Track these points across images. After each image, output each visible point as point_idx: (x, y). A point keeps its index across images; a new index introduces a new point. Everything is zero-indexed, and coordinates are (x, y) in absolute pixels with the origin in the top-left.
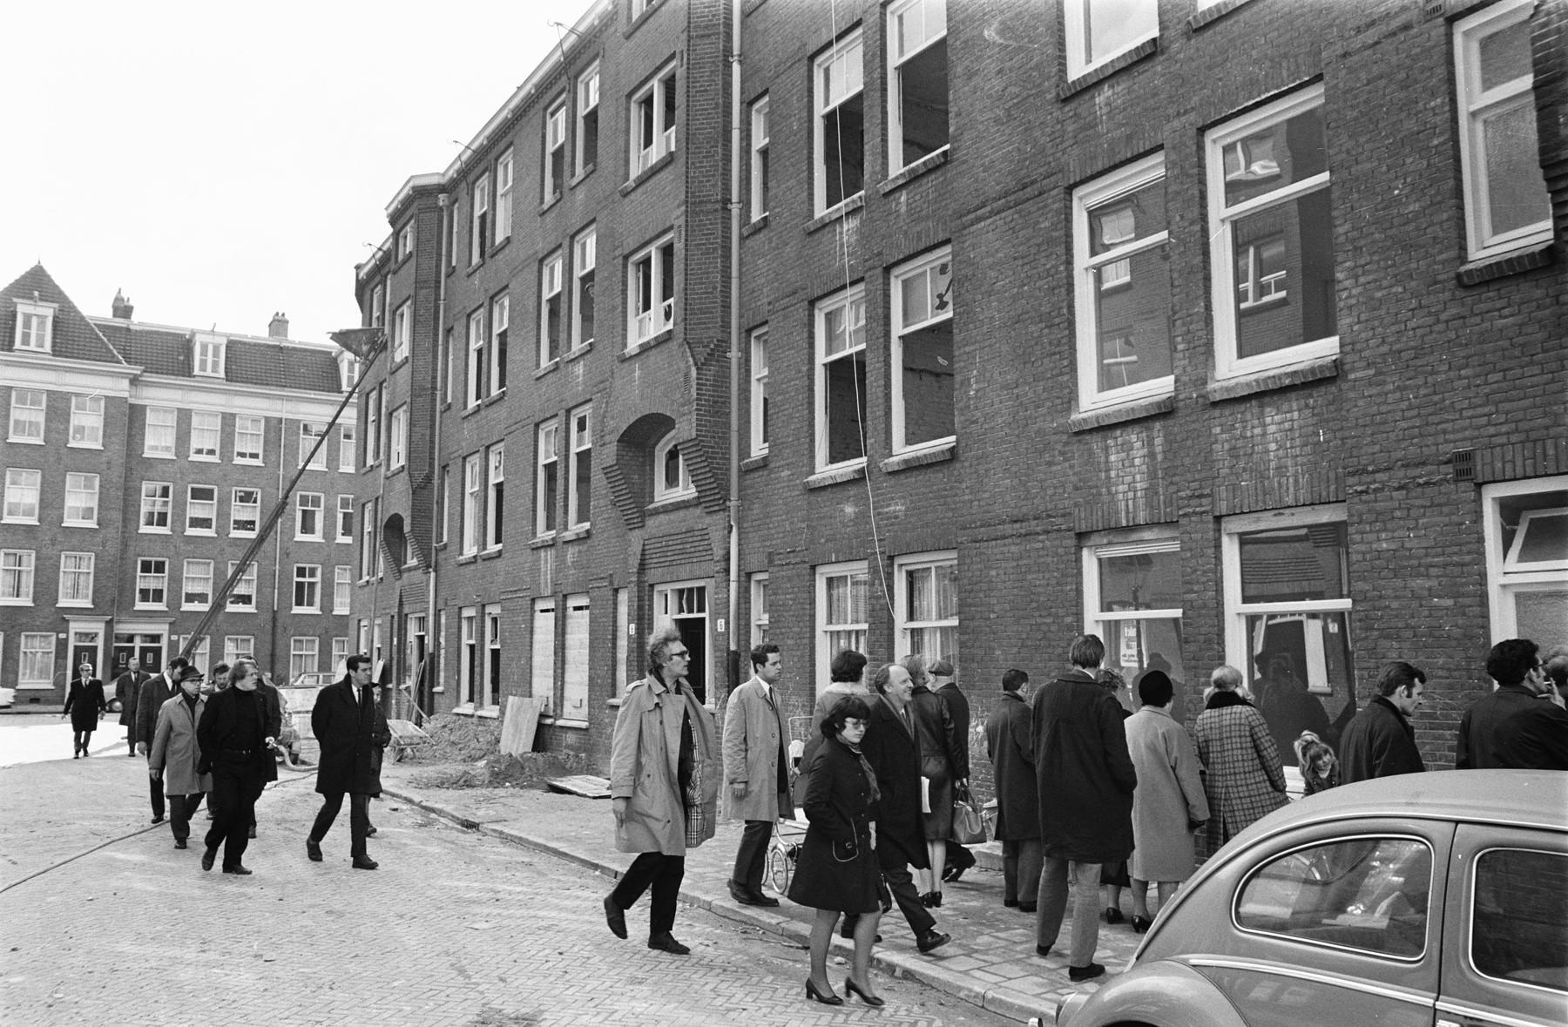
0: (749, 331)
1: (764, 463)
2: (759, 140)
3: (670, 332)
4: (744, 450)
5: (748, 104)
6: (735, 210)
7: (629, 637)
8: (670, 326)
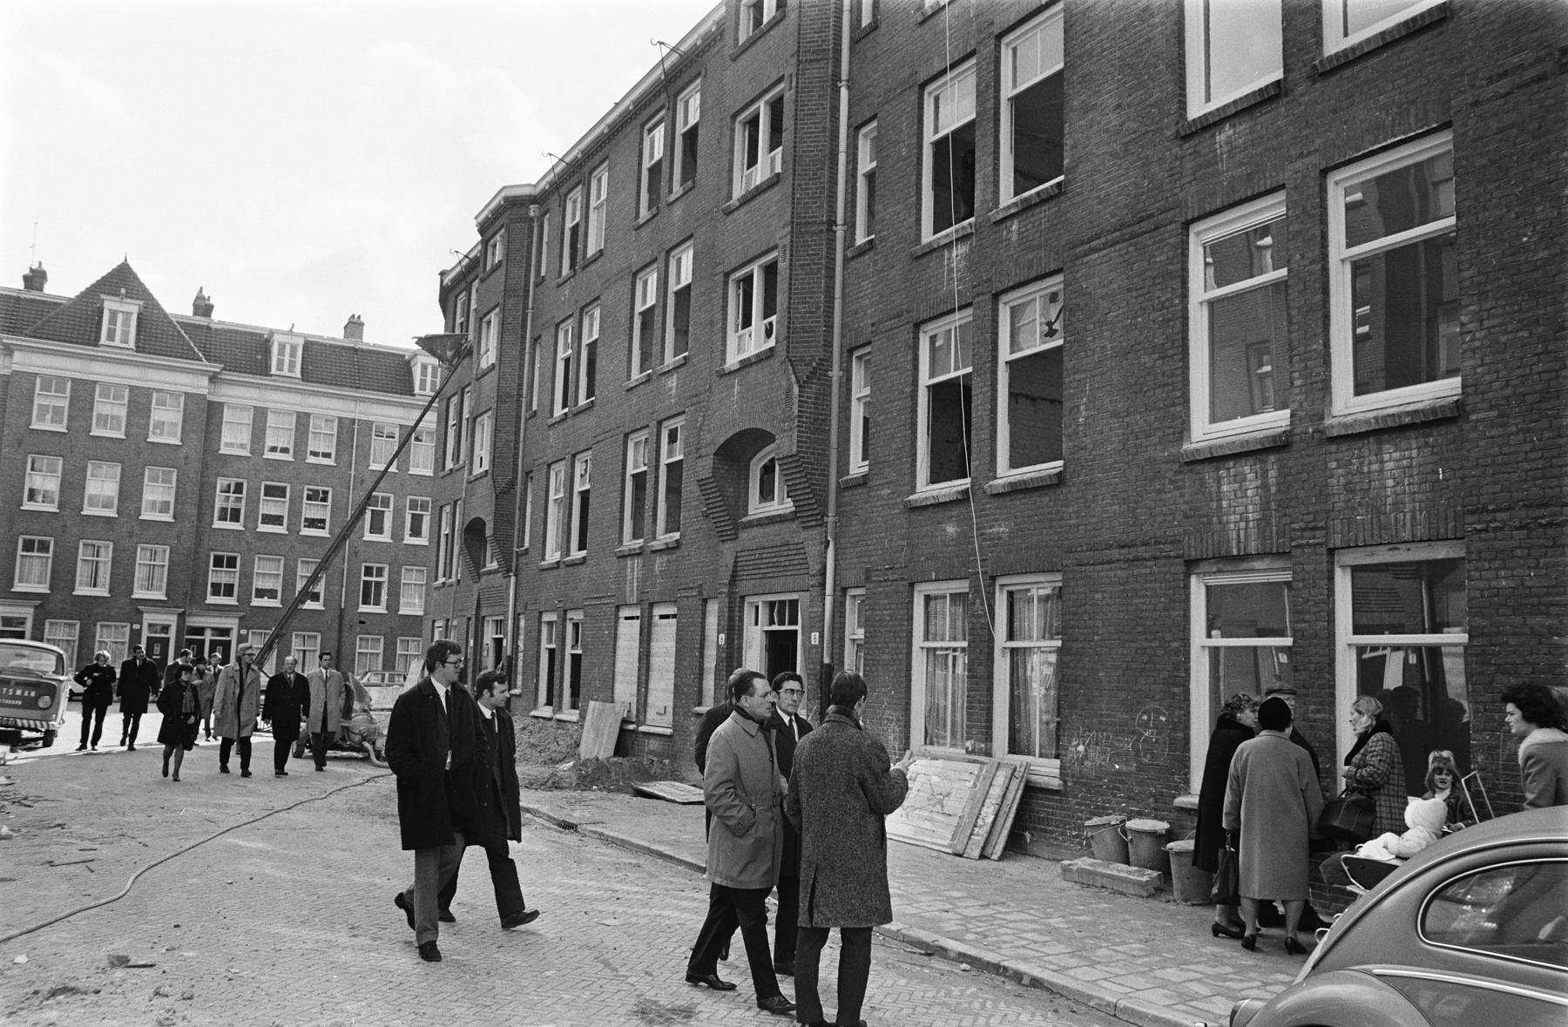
0: (851, 351)
1: (863, 481)
2: (865, 165)
4: (843, 467)
5: (855, 129)
6: (840, 232)
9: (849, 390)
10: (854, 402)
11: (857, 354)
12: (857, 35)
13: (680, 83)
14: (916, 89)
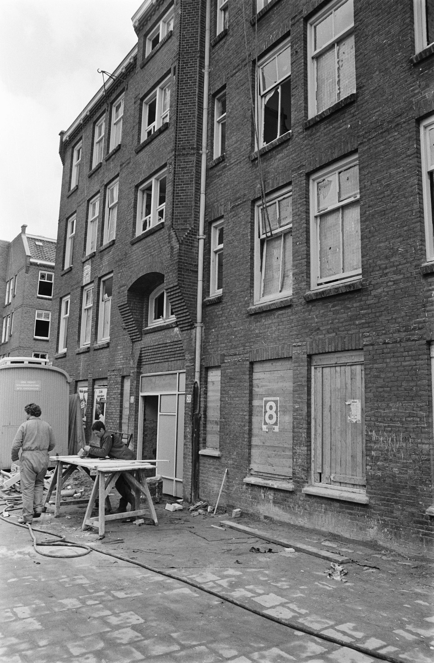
0: (210, 223)
1: (219, 300)
2: (215, 246)
3: (163, 223)
4: (206, 291)
5: (208, 224)
6: (204, 151)
7: (130, 404)
8: (163, 221)
9: (213, 116)
10: (212, 254)
11: (214, 225)
12: (212, 164)
13: (112, 98)
14: (249, 203)
